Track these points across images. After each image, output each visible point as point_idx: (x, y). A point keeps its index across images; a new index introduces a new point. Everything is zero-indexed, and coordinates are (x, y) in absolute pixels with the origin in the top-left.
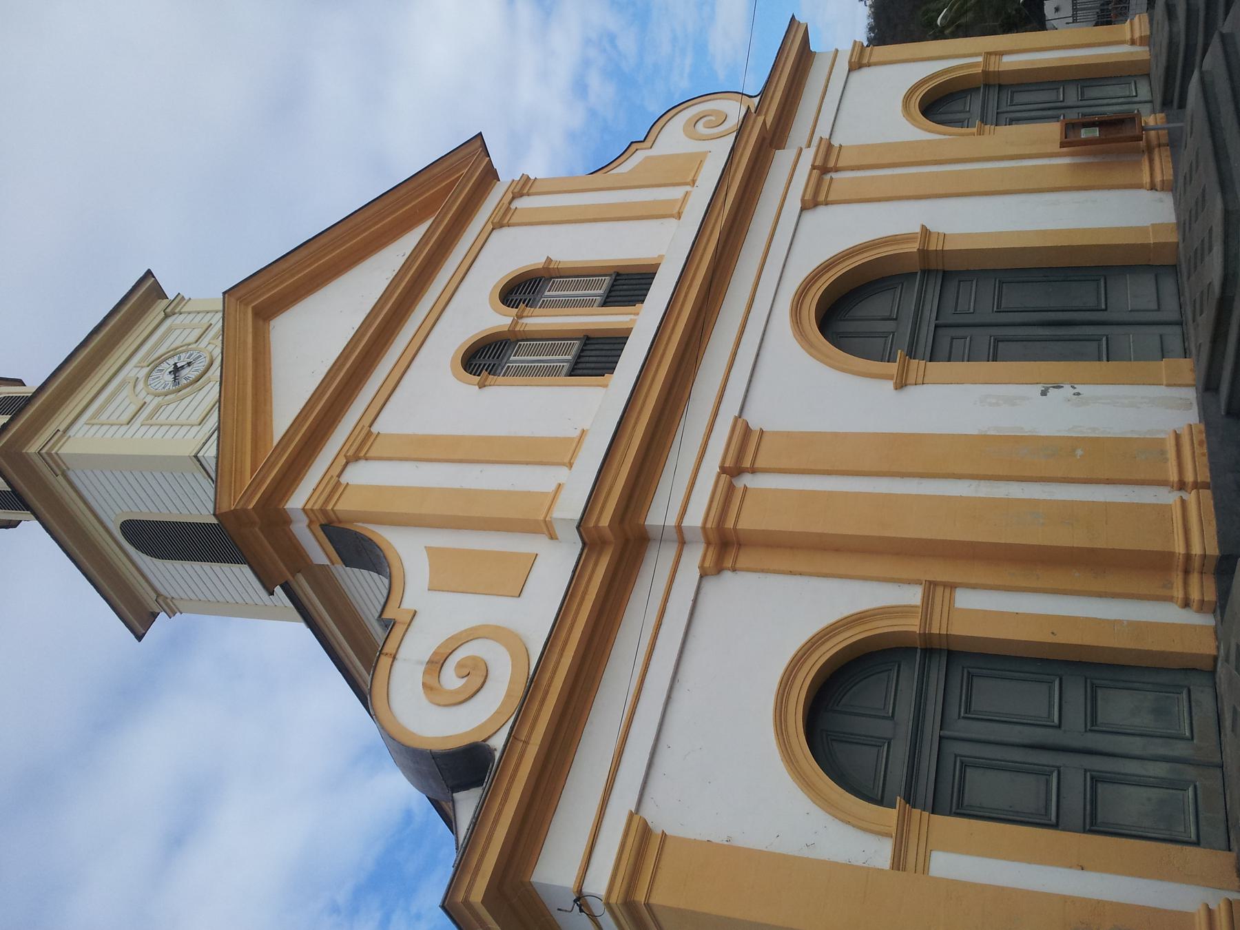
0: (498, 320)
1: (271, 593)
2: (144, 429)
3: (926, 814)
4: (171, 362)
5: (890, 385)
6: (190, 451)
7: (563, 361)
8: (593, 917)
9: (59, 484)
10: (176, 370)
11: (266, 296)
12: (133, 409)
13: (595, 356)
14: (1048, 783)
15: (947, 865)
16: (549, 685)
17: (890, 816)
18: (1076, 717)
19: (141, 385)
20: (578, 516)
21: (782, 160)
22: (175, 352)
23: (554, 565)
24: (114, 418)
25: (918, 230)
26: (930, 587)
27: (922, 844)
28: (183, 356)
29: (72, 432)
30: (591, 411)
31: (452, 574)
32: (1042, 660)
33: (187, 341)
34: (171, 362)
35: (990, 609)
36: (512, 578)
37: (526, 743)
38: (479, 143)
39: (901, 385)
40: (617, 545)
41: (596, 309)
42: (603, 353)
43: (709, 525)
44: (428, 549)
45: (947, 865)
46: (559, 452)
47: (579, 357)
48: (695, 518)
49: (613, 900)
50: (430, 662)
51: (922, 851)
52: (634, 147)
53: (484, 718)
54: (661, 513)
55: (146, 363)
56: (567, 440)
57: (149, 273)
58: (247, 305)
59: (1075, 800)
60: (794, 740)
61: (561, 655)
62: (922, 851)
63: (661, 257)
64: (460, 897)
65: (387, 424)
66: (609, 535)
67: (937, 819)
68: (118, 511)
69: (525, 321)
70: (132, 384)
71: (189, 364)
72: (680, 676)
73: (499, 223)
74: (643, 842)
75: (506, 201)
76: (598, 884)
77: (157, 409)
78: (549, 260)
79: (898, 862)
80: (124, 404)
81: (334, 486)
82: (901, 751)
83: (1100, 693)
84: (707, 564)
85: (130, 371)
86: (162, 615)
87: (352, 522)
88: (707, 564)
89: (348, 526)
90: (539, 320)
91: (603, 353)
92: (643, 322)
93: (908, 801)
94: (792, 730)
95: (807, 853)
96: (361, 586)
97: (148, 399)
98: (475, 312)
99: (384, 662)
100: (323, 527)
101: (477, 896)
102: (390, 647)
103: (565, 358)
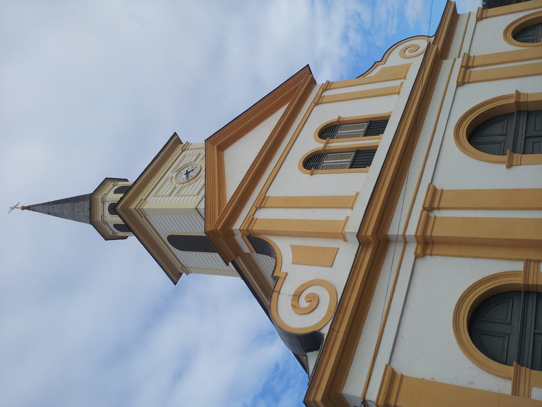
0: (318, 145)
2: (176, 197)
3: (528, 370)
4: (185, 170)
5: (504, 166)
6: (194, 206)
9: (143, 221)
10: (187, 173)
11: (222, 140)
12: (171, 189)
13: (361, 159)
16: (347, 307)
19: (174, 180)
21: (446, 64)
22: (186, 166)
23: (347, 253)
25: (514, 92)
29: (148, 200)
31: (302, 257)
34: (185, 170)
36: (328, 259)
37: (338, 332)
40: (375, 243)
44: (292, 246)
46: (346, 203)
47: (354, 159)
48: (412, 231)
50: (294, 295)
52: (377, 64)
54: (395, 229)
56: (351, 197)
57: (175, 134)
58: (214, 145)
63: (391, 112)
64: (311, 399)
65: (272, 193)
66: (371, 239)
67: (533, 372)
68: (166, 232)
69: (329, 145)
70: (170, 180)
71: (192, 170)
74: (392, 379)
75: (320, 93)
77: (181, 188)
78: (339, 117)
79: (515, 391)
80: (167, 188)
81: (252, 220)
82: (515, 339)
88: (418, 252)
89: (258, 236)
90: (336, 144)
92: (383, 142)
96: (264, 262)
97: (177, 185)
98: (308, 142)
99: (275, 295)
100: (248, 237)
102: (277, 289)
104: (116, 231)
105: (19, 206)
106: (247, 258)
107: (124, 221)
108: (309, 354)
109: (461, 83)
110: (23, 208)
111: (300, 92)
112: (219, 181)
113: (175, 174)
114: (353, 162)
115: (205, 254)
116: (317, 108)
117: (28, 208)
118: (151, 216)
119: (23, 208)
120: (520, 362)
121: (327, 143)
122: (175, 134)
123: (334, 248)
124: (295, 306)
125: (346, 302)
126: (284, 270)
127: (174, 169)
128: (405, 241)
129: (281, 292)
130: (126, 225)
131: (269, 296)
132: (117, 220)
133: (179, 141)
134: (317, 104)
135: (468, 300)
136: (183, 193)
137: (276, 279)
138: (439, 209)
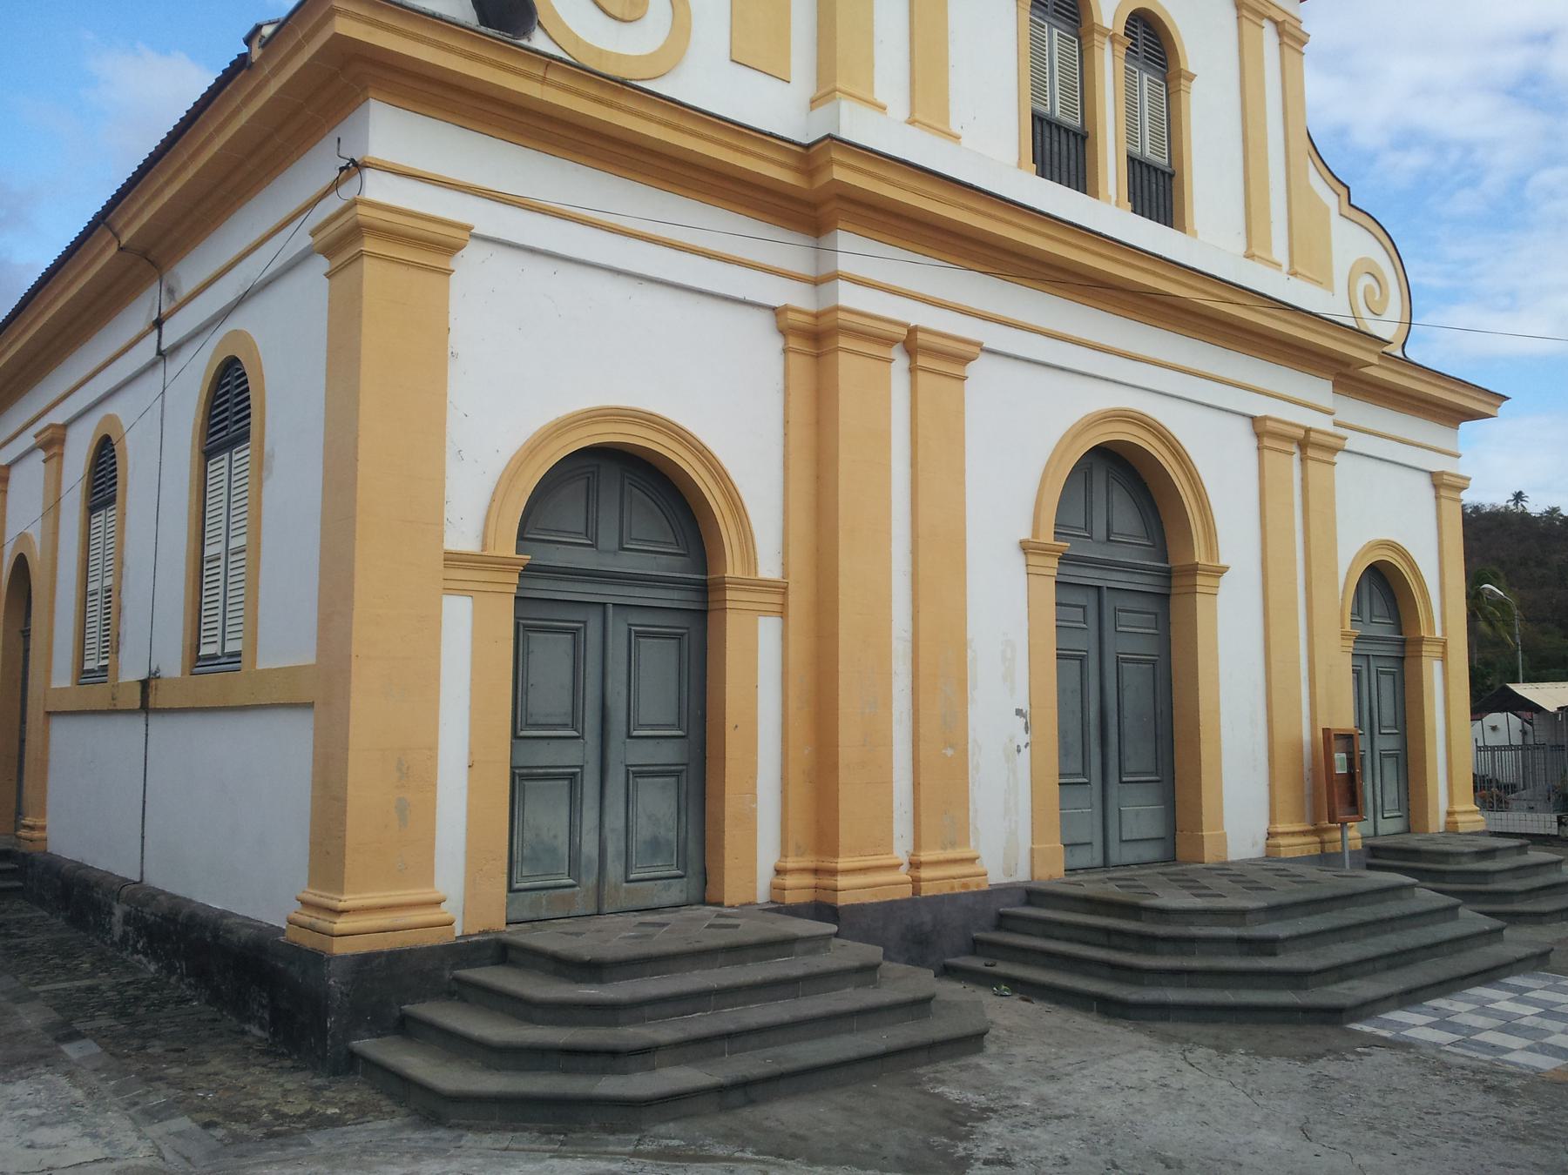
5: (1026, 534)
7: (1052, 104)
8: (335, 185)
13: (1061, 148)
14: (564, 726)
15: (458, 614)
16: (620, 108)
17: (506, 546)
18: (642, 754)
21: (1319, 389)
23: (776, 106)
25: (1223, 562)
26: (782, 589)
32: (704, 716)
35: (759, 659)
37: (543, 81)
39: (1026, 548)
40: (809, 193)
41: (1124, 147)
42: (1064, 161)
43: (841, 315)
45: (458, 614)
46: (928, 105)
47: (1059, 127)
48: (849, 296)
49: (360, 209)
52: (1343, 192)
54: (854, 251)
59: (546, 756)
63: (1195, 234)
69: (1108, 47)
72: (646, 285)
74: (437, 245)
78: (1191, 77)
79: (454, 560)
84: (790, 315)
88: (790, 315)
90: (1109, 64)
92: (1107, 212)
103: (1057, 109)
109: (1261, 428)
114: (1050, 123)
120: (529, 571)
125: (631, 104)
128: (821, 280)
138: (913, 370)
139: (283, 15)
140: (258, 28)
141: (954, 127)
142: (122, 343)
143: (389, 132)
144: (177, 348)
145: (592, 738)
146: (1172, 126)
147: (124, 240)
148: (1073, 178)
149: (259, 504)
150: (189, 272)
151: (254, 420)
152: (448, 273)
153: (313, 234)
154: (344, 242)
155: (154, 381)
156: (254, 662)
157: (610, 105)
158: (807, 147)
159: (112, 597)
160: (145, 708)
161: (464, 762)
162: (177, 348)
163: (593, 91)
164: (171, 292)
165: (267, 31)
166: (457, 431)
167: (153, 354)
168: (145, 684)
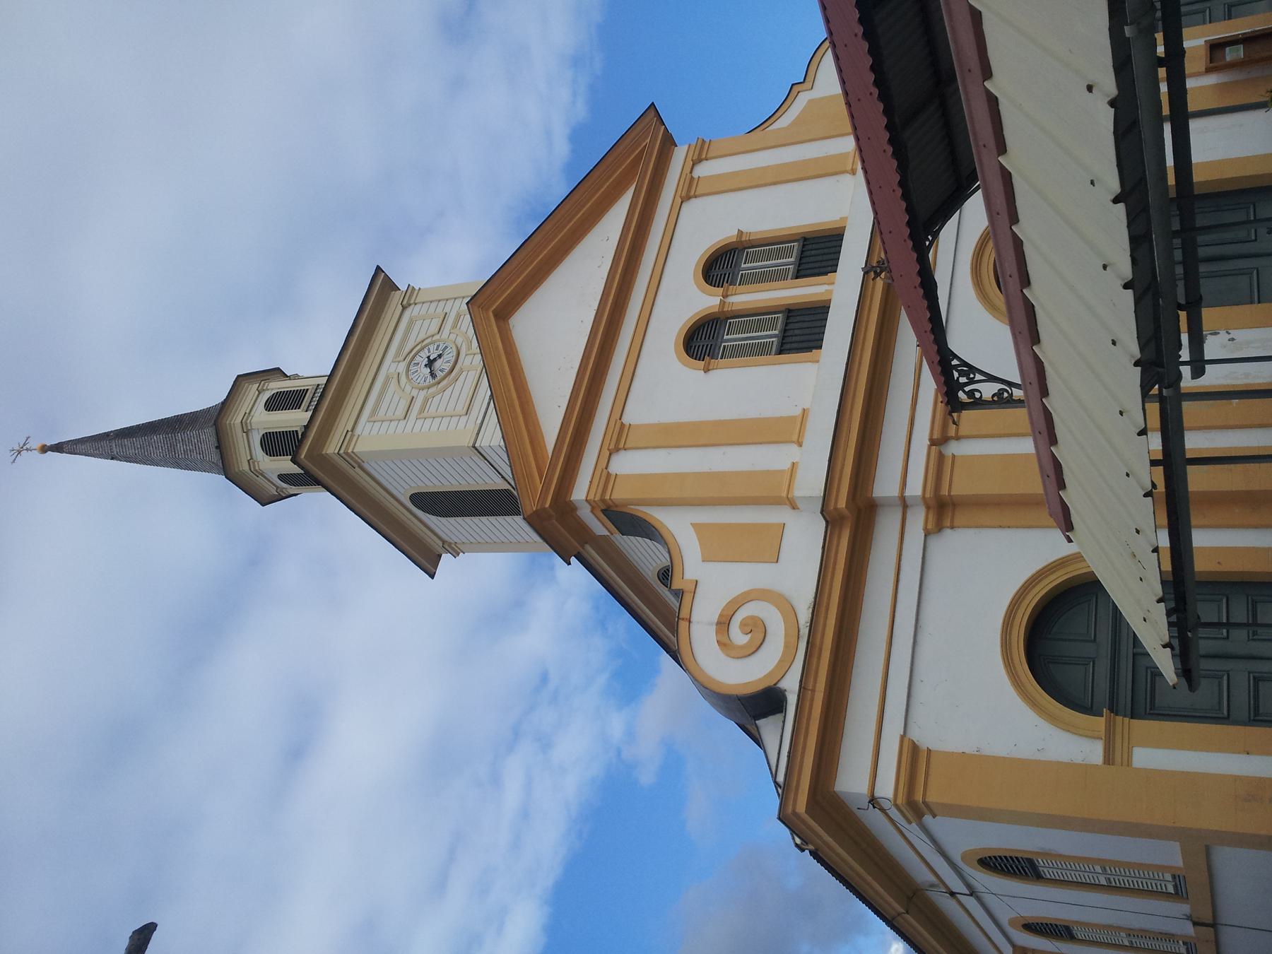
0: (706, 301)
1: (569, 564)
2: (420, 422)
3: (1126, 720)
4: (424, 354)
6: (467, 441)
7: (771, 336)
8: (883, 810)
9: (357, 474)
10: (430, 363)
11: (499, 299)
12: (403, 405)
13: (800, 331)
14: (1220, 685)
15: (1145, 757)
16: (822, 643)
17: (1099, 723)
19: (403, 379)
20: (820, 491)
22: (422, 345)
23: (804, 540)
24: (390, 414)
27: (1126, 744)
28: (431, 347)
29: (358, 430)
30: (810, 387)
31: (722, 546)
32: (1211, 583)
33: (430, 333)
34: (424, 354)
36: (766, 545)
37: (813, 691)
38: (653, 113)
40: (853, 518)
41: (790, 282)
42: (806, 325)
43: (928, 495)
44: (696, 526)
45: (1145, 757)
46: (787, 430)
47: (785, 330)
48: (915, 488)
49: (899, 802)
50: (719, 623)
51: (1125, 749)
52: (796, 89)
53: (770, 666)
54: (885, 486)
55: (401, 358)
56: (791, 419)
57: (378, 269)
58: (487, 310)
59: (1242, 697)
60: (1015, 651)
61: (826, 618)
62: (1125, 749)
63: (844, 219)
64: (790, 810)
65: (634, 415)
66: (846, 512)
67: (1135, 722)
68: (407, 487)
69: (731, 299)
70: (394, 381)
71: (440, 356)
72: (921, 623)
73: (689, 192)
74: (914, 758)
75: (687, 170)
76: (886, 788)
77: (426, 400)
78: (740, 233)
79: (1109, 758)
80: (394, 401)
81: (606, 478)
82: (1103, 667)
83: (1260, 607)
84: (930, 527)
85: (390, 367)
86: (446, 558)
87: (626, 505)
88: (930, 527)
89: (624, 510)
90: (745, 298)
91: (806, 325)
92: (843, 289)
93: (1111, 710)
94: (1016, 661)
95: (1040, 757)
96: (638, 550)
97: (415, 393)
98: (684, 297)
99: (683, 625)
100: (604, 511)
101: (801, 807)
102: (684, 613)
103: (771, 335)
104: (285, 485)
105: (35, 444)
106: (605, 547)
107: (302, 468)
108: (760, 722)
110: (44, 449)
111: (646, 172)
112: (519, 398)
113: (403, 365)
115: (492, 519)
116: (690, 209)
117: (58, 448)
118: (373, 464)
119: (44, 449)
120: (1114, 709)
121: (725, 296)
122: (378, 269)
123: (778, 525)
124: (725, 645)
125: (819, 636)
126: (689, 575)
127: (398, 354)
128: (904, 504)
129: (694, 619)
130: (307, 472)
131: (674, 630)
132: (285, 464)
133: (390, 286)
134: (687, 198)
135: (1026, 601)
136: (433, 409)
137: (679, 594)
138: (958, 438)
139: (788, 831)
140: (797, 845)
141: (798, 412)
142: (980, 933)
143: (852, 780)
144: (968, 886)
145: (1230, 665)
146: (771, 244)
147: (902, 910)
148: (818, 317)
149: (1069, 857)
150: (922, 875)
151: (1019, 855)
152: (929, 751)
153: (910, 823)
154: (916, 809)
155: (988, 899)
156: (1179, 868)
157: (821, 650)
158: (827, 522)
159: (1130, 932)
160: (1214, 925)
161: (1244, 757)
162: (968, 886)
163: (815, 661)
164: (932, 885)
165: (798, 841)
166: (1026, 751)
167: (972, 899)
168: (1195, 924)
